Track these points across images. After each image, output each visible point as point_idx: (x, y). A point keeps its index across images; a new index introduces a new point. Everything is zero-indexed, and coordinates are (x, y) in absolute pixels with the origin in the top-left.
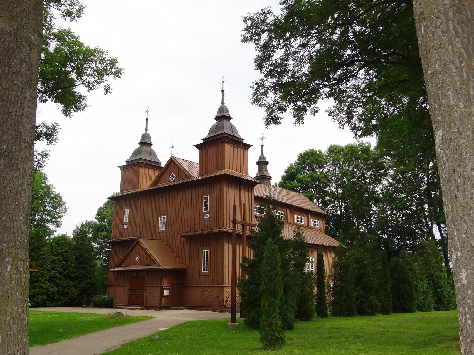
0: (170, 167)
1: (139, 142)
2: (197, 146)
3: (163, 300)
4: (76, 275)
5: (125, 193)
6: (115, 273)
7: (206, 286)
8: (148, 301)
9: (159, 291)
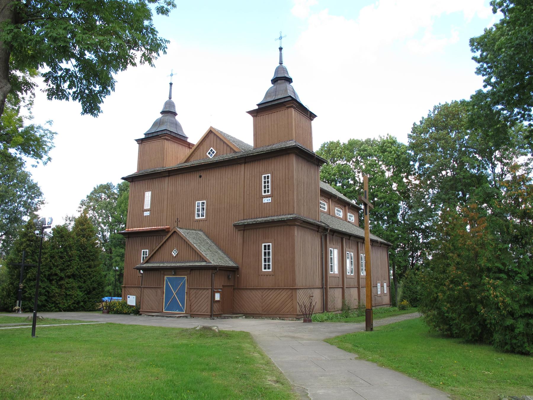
1: (161, 111)
2: (250, 112)
3: (216, 306)
4: (61, 274)
5: (143, 172)
7: (269, 289)
8: (192, 308)
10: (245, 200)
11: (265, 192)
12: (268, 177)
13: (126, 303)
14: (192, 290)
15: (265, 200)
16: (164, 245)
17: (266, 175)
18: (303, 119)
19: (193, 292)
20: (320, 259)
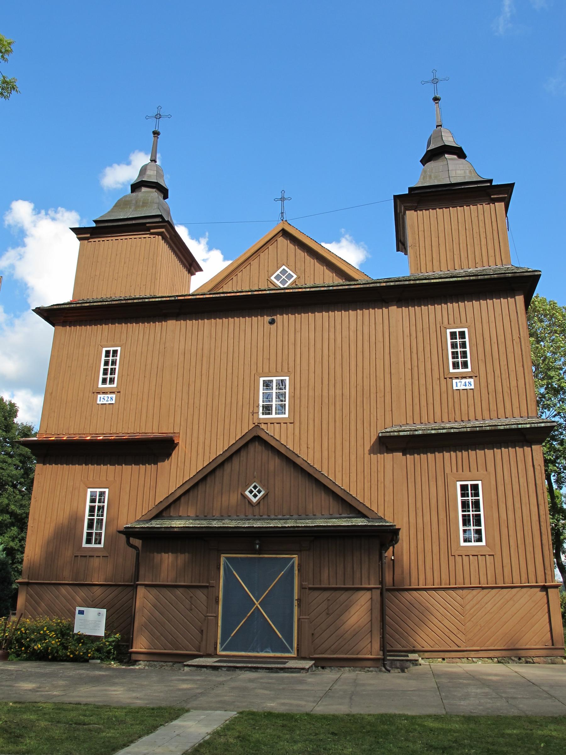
11: (104, 381)
12: (462, 335)
13: (71, 627)
16: (218, 473)
17: (112, 349)
19: (319, 600)
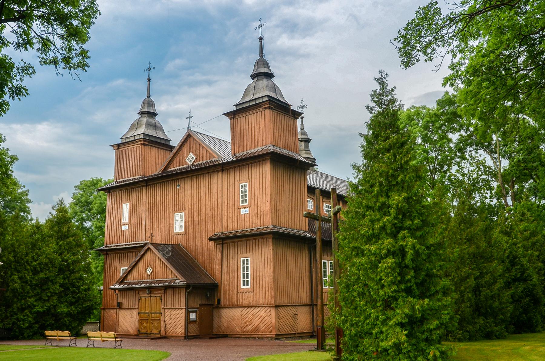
0: (187, 144)
1: (138, 111)
6: (117, 291)
9: (183, 315)
10: (223, 211)
14: (166, 311)
15: (243, 211)
18: (286, 121)
20: (307, 273)
